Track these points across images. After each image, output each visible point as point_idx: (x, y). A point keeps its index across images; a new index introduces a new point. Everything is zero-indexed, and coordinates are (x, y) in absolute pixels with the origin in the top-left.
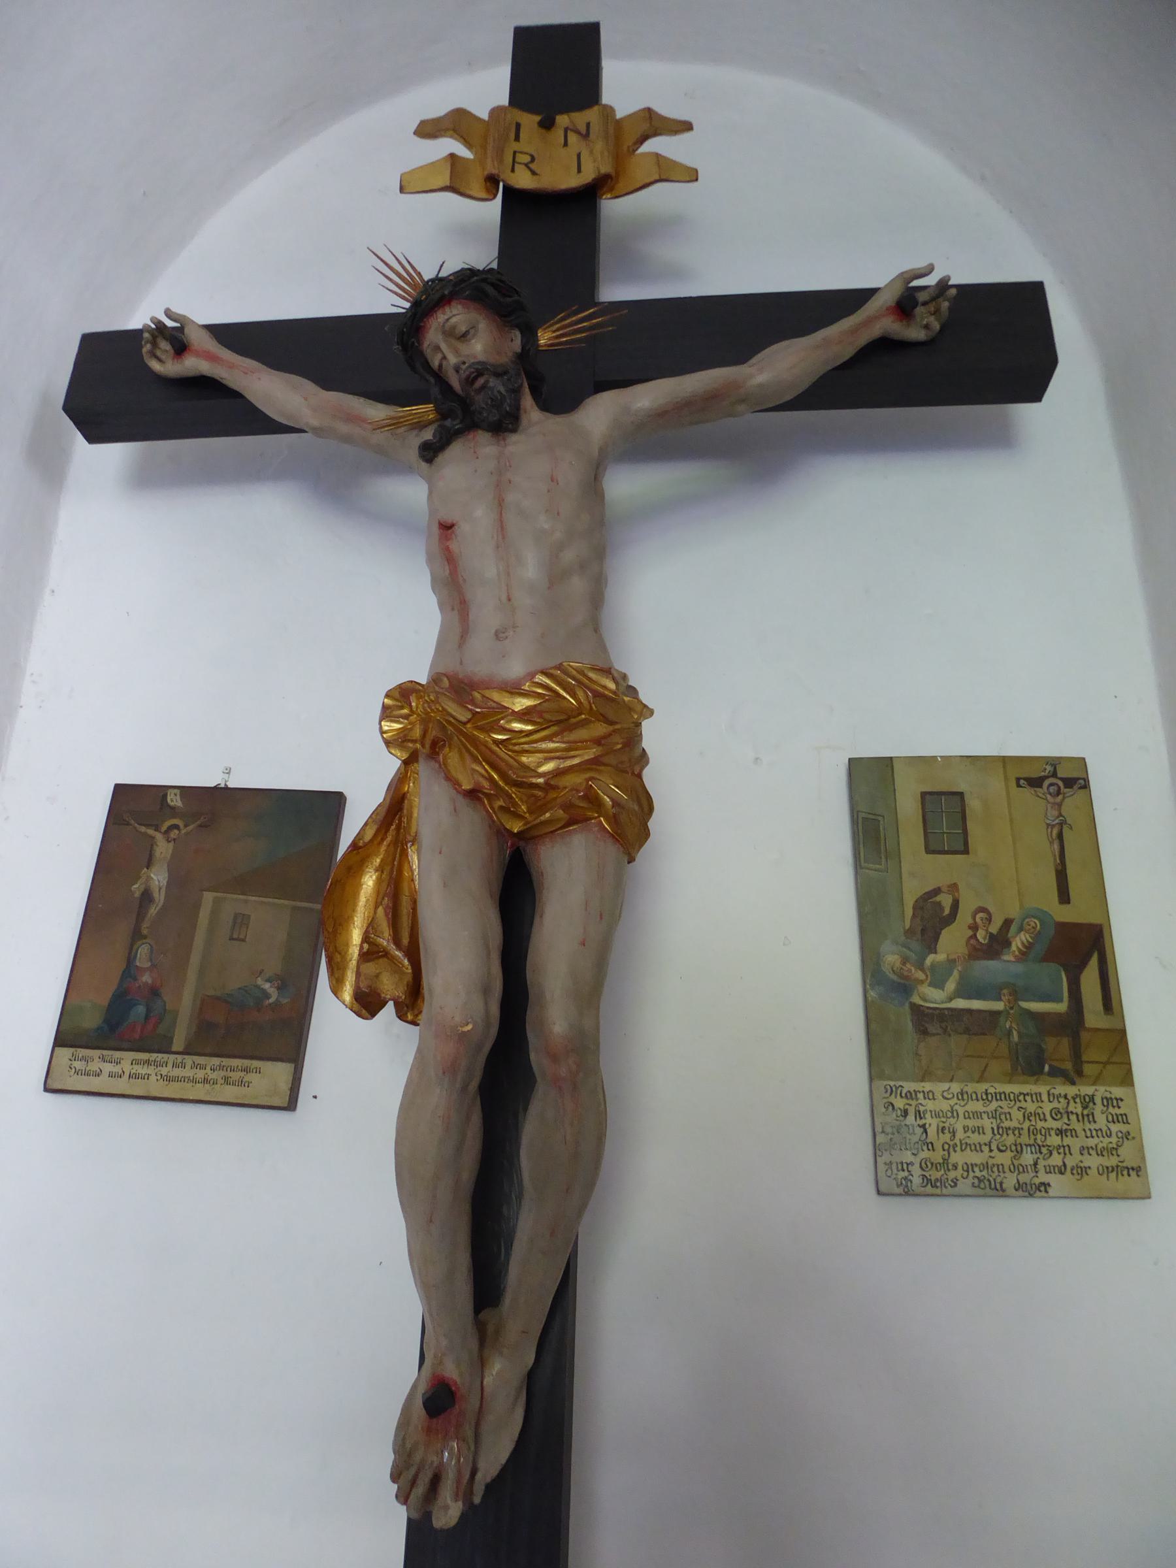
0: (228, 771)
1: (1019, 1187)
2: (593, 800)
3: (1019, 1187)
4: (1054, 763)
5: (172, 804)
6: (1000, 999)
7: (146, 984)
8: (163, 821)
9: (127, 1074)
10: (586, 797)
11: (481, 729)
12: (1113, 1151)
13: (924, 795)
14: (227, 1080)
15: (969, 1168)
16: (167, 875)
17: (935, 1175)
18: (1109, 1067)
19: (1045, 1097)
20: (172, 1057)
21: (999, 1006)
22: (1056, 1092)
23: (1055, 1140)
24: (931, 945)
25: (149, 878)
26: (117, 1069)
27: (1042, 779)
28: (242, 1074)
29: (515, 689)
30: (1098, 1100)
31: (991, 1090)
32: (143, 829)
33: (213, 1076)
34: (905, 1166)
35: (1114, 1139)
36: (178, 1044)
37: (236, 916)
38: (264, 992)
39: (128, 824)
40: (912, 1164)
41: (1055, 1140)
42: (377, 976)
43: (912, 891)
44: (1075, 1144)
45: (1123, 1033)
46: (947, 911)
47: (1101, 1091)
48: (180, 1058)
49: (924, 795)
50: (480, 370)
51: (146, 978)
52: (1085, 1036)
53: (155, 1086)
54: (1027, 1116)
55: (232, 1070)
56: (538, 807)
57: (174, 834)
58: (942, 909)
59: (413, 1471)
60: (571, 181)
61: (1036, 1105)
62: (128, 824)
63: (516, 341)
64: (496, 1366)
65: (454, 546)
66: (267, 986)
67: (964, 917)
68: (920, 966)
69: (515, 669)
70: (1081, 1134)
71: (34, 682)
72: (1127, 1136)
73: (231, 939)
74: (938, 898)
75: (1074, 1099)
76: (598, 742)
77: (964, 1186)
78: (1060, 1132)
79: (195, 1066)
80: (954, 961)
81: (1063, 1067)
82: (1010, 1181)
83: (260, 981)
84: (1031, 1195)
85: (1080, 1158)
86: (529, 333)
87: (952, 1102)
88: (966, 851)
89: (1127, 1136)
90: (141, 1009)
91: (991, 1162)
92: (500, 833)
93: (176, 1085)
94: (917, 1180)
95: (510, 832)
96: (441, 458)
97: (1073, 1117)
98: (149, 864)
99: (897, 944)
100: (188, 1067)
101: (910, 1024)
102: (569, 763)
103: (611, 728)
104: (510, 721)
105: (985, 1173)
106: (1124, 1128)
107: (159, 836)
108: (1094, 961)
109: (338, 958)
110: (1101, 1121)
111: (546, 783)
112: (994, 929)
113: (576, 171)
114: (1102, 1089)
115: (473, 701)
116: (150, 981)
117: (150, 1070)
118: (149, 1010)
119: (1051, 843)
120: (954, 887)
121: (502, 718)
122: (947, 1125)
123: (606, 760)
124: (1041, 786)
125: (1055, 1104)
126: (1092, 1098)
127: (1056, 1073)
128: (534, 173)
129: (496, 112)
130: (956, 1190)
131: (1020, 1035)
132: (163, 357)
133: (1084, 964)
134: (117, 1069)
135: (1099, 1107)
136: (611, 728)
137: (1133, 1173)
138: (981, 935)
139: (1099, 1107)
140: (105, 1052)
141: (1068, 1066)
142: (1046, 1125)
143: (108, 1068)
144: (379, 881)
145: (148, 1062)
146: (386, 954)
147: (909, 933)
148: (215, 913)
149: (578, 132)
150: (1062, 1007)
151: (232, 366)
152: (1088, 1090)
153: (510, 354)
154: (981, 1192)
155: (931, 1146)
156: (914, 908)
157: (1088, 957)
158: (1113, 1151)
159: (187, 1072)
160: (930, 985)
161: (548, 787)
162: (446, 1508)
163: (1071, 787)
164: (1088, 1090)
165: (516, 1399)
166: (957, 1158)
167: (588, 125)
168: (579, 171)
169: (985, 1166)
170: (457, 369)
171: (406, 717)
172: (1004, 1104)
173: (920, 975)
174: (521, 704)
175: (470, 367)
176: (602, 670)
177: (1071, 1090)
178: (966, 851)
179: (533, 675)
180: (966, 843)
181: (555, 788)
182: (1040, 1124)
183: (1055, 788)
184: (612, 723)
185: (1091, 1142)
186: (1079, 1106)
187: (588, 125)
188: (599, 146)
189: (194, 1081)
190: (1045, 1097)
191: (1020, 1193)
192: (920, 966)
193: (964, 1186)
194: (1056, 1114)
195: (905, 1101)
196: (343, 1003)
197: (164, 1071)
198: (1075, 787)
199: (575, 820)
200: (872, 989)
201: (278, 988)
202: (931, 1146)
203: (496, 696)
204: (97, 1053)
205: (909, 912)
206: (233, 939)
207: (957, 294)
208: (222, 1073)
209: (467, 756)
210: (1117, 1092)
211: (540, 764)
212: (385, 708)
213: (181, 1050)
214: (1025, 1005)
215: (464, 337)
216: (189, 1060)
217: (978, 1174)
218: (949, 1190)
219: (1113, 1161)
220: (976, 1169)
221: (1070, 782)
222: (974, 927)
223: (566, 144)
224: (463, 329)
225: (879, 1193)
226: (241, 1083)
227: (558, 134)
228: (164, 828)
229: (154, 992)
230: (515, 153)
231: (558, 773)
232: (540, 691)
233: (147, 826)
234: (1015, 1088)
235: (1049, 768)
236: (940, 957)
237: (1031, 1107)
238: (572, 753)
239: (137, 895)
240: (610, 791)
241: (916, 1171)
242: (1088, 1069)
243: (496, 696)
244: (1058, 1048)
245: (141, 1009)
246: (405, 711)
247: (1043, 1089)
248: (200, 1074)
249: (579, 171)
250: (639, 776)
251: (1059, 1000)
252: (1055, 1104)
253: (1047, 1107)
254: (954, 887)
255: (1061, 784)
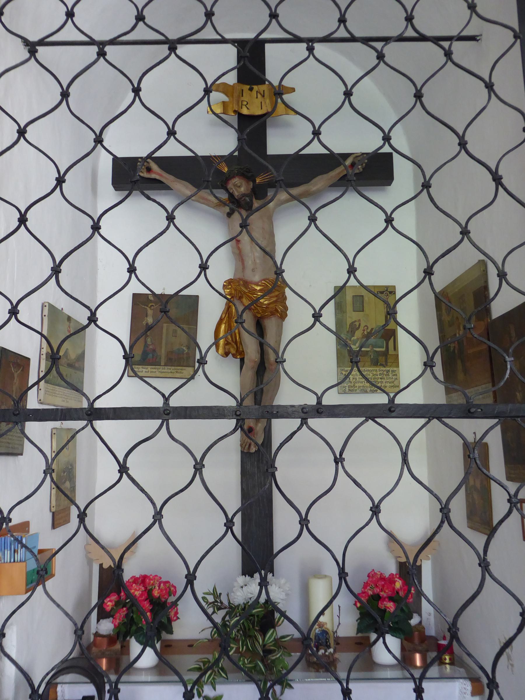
0: (164, 289)
1: (371, 391)
2: (277, 310)
3: (371, 391)
4: (387, 287)
5: (151, 299)
6: (369, 348)
7: (151, 349)
8: (149, 304)
9: (150, 372)
10: (275, 310)
11: (251, 294)
12: (393, 382)
13: (353, 296)
14: (177, 372)
15: (359, 387)
16: (152, 319)
17: (351, 389)
18: (394, 363)
19: (378, 371)
20: (162, 367)
21: (369, 349)
22: (381, 369)
23: (380, 380)
24: (353, 336)
25: (147, 320)
26: (147, 370)
27: (384, 292)
28: (181, 370)
29: (257, 285)
30: (390, 371)
31: (366, 369)
32: (143, 306)
33: (173, 371)
34: (345, 387)
35: (393, 380)
36: (162, 363)
37: (173, 330)
38: (183, 350)
39: (138, 305)
40: (346, 386)
41: (380, 380)
42: (229, 348)
43: (349, 321)
44: (384, 381)
45: (398, 355)
46: (357, 326)
47: (391, 369)
48: (164, 367)
49: (353, 296)
50: (244, 195)
51: (151, 347)
52: (388, 356)
53: (158, 374)
54: (374, 375)
55: (178, 369)
56: (264, 311)
57: (152, 308)
58: (356, 326)
59: (245, 443)
60: (259, 112)
61: (375, 372)
62: (138, 305)
63: (251, 185)
64: (260, 425)
65: (240, 246)
66: (184, 348)
67: (362, 328)
68: (350, 340)
69: (257, 278)
70: (386, 379)
71: (101, 261)
72: (396, 379)
73: (173, 336)
74: (355, 323)
75: (385, 371)
76: (276, 296)
77: (358, 391)
78: (381, 378)
79: (168, 369)
80: (358, 339)
81: (383, 363)
82: (369, 390)
83: (182, 347)
84: (373, 393)
85: (385, 384)
86: (254, 181)
87: (356, 372)
88: (363, 311)
89: (396, 379)
90: (151, 355)
91: (364, 385)
92: (255, 316)
93: (164, 374)
94: (347, 390)
95: (258, 317)
96: (232, 216)
97: (384, 375)
98: (147, 316)
99: (345, 335)
100: (166, 369)
101: (347, 354)
102: (270, 301)
103: (279, 293)
104: (258, 293)
105: (363, 388)
106: (395, 377)
107: (148, 308)
108: (392, 338)
109: (217, 344)
110: (391, 375)
111: (266, 307)
112: (369, 331)
113: (260, 108)
114: (391, 368)
115: (249, 288)
116: (152, 348)
117: (156, 370)
118: (153, 356)
119: (385, 309)
120: (359, 320)
121: (256, 292)
122: (355, 377)
123: (278, 300)
124: (383, 294)
125: (380, 372)
126: (389, 371)
127: (381, 365)
128: (248, 109)
129: (234, 84)
130: (356, 392)
131: (373, 356)
132: (143, 171)
133: (390, 339)
134: (147, 370)
135: (390, 372)
136: (279, 293)
137: (397, 387)
138: (365, 332)
139: (390, 372)
140: (143, 366)
141: (384, 363)
142: (378, 377)
143: (144, 370)
144: (225, 327)
145: (155, 368)
146: (230, 343)
147: (348, 332)
148: (167, 329)
149: (261, 94)
150: (384, 349)
151: (166, 179)
152: (388, 369)
153: (250, 189)
154: (362, 392)
155: (351, 382)
156: (349, 325)
157: (391, 337)
158: (393, 382)
159: (166, 371)
160: (352, 345)
161: (266, 308)
162: (253, 449)
163: (391, 294)
164: (388, 369)
165: (263, 432)
166: (357, 385)
167: (264, 91)
168: (262, 109)
169: (363, 386)
170: (238, 196)
171: (230, 288)
172: (368, 372)
173: (350, 342)
174: (258, 288)
175: (241, 195)
176: (264, 251)
177: (384, 369)
178: (363, 311)
179: (262, 280)
180: (363, 309)
181: (268, 308)
182: (376, 377)
183: (387, 294)
184: (279, 291)
185: (388, 380)
186: (386, 373)
187: (264, 91)
188: (268, 101)
189: (168, 373)
190: (378, 371)
191: (371, 392)
192: (350, 340)
193: (358, 391)
194: (380, 374)
195: (345, 372)
196: (219, 354)
197: (160, 370)
198: (392, 294)
199: (273, 314)
200: (338, 346)
201: (187, 349)
202: (351, 382)
203: (253, 286)
204: (141, 366)
205: (348, 327)
206: (174, 336)
207: (367, 162)
208: (175, 370)
209: (247, 300)
210: (395, 369)
211: (264, 302)
212: (224, 286)
213: (163, 365)
214: (375, 349)
215: (239, 187)
216: (166, 367)
217: (361, 388)
218: (355, 392)
219: (393, 384)
220: (361, 387)
221: (391, 292)
222: (364, 330)
223: (257, 98)
224: (239, 185)
225: (338, 393)
226: (181, 373)
227: (254, 92)
228: (149, 306)
229: (154, 350)
230: (242, 101)
231: (269, 304)
232: (263, 284)
233: (145, 305)
234: (371, 369)
235: (386, 289)
236: (355, 338)
237: (375, 373)
238: (271, 299)
239: (145, 325)
240: (280, 308)
241: (347, 388)
242: (388, 364)
243: (253, 286)
244: (382, 359)
245: (151, 355)
246: (230, 287)
247: (378, 369)
248: (170, 371)
249: (262, 109)
250: (285, 303)
251: (383, 348)
252: (380, 372)
253: (378, 373)
254: (359, 320)
255: (388, 293)
